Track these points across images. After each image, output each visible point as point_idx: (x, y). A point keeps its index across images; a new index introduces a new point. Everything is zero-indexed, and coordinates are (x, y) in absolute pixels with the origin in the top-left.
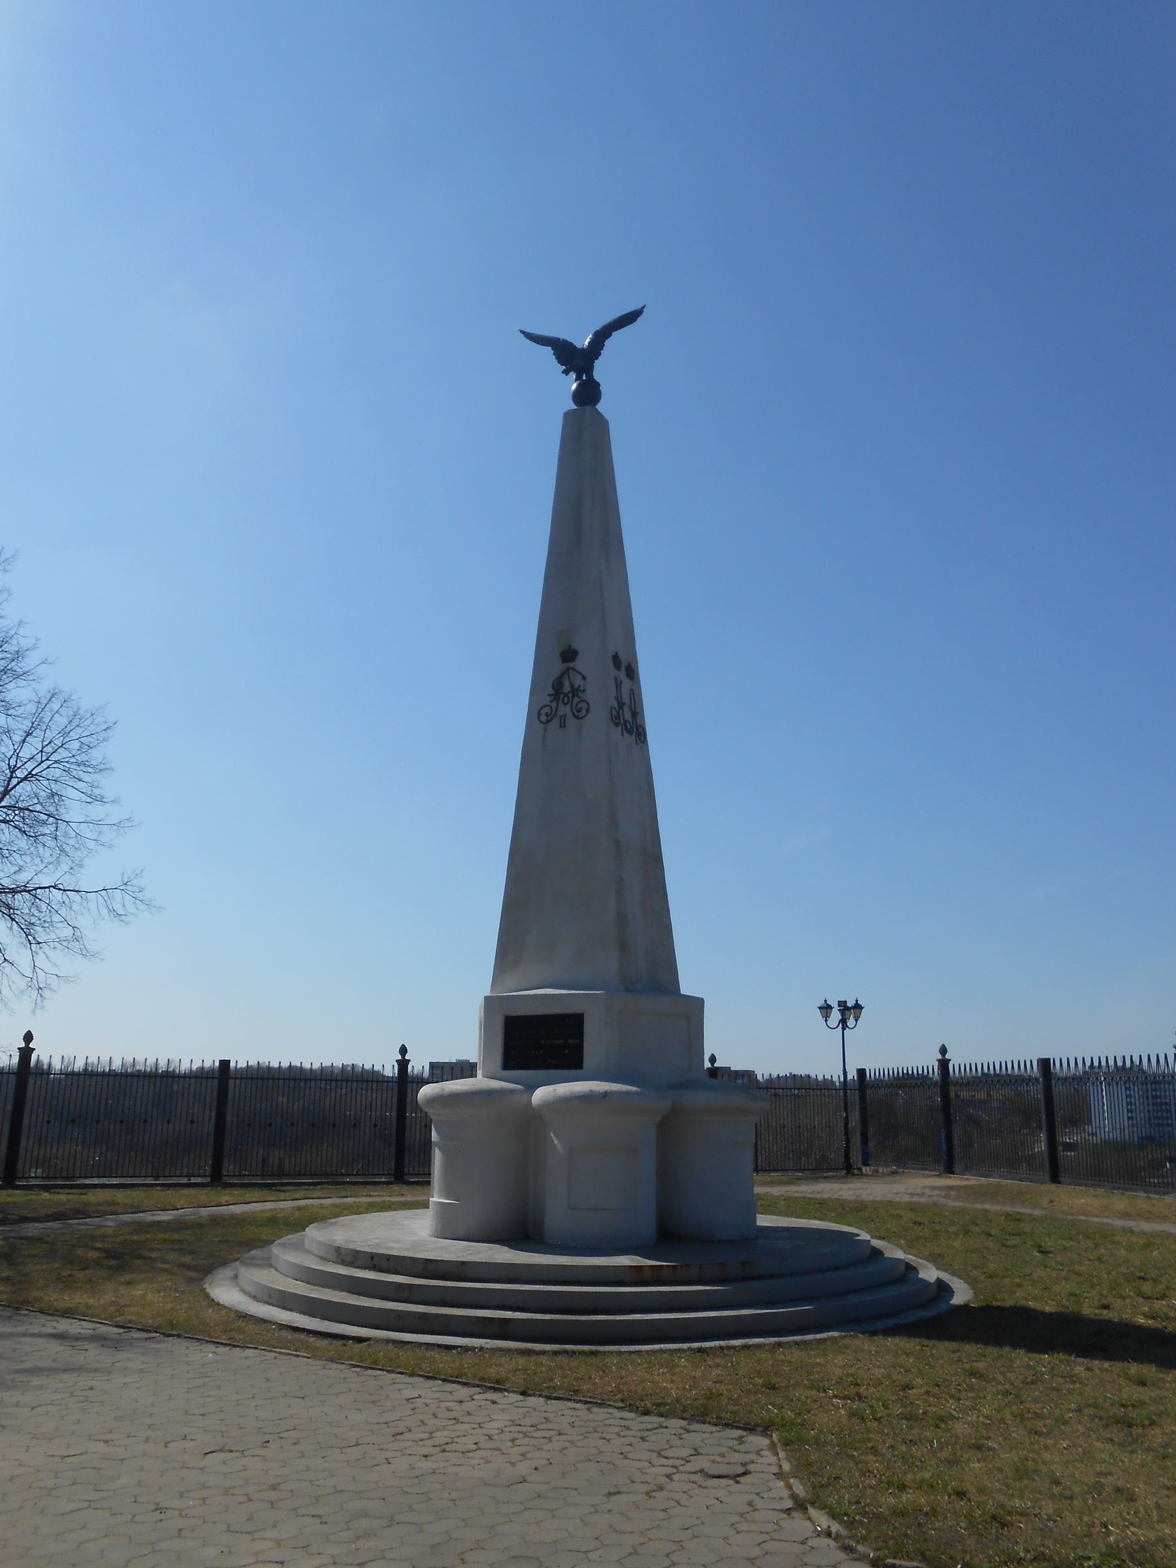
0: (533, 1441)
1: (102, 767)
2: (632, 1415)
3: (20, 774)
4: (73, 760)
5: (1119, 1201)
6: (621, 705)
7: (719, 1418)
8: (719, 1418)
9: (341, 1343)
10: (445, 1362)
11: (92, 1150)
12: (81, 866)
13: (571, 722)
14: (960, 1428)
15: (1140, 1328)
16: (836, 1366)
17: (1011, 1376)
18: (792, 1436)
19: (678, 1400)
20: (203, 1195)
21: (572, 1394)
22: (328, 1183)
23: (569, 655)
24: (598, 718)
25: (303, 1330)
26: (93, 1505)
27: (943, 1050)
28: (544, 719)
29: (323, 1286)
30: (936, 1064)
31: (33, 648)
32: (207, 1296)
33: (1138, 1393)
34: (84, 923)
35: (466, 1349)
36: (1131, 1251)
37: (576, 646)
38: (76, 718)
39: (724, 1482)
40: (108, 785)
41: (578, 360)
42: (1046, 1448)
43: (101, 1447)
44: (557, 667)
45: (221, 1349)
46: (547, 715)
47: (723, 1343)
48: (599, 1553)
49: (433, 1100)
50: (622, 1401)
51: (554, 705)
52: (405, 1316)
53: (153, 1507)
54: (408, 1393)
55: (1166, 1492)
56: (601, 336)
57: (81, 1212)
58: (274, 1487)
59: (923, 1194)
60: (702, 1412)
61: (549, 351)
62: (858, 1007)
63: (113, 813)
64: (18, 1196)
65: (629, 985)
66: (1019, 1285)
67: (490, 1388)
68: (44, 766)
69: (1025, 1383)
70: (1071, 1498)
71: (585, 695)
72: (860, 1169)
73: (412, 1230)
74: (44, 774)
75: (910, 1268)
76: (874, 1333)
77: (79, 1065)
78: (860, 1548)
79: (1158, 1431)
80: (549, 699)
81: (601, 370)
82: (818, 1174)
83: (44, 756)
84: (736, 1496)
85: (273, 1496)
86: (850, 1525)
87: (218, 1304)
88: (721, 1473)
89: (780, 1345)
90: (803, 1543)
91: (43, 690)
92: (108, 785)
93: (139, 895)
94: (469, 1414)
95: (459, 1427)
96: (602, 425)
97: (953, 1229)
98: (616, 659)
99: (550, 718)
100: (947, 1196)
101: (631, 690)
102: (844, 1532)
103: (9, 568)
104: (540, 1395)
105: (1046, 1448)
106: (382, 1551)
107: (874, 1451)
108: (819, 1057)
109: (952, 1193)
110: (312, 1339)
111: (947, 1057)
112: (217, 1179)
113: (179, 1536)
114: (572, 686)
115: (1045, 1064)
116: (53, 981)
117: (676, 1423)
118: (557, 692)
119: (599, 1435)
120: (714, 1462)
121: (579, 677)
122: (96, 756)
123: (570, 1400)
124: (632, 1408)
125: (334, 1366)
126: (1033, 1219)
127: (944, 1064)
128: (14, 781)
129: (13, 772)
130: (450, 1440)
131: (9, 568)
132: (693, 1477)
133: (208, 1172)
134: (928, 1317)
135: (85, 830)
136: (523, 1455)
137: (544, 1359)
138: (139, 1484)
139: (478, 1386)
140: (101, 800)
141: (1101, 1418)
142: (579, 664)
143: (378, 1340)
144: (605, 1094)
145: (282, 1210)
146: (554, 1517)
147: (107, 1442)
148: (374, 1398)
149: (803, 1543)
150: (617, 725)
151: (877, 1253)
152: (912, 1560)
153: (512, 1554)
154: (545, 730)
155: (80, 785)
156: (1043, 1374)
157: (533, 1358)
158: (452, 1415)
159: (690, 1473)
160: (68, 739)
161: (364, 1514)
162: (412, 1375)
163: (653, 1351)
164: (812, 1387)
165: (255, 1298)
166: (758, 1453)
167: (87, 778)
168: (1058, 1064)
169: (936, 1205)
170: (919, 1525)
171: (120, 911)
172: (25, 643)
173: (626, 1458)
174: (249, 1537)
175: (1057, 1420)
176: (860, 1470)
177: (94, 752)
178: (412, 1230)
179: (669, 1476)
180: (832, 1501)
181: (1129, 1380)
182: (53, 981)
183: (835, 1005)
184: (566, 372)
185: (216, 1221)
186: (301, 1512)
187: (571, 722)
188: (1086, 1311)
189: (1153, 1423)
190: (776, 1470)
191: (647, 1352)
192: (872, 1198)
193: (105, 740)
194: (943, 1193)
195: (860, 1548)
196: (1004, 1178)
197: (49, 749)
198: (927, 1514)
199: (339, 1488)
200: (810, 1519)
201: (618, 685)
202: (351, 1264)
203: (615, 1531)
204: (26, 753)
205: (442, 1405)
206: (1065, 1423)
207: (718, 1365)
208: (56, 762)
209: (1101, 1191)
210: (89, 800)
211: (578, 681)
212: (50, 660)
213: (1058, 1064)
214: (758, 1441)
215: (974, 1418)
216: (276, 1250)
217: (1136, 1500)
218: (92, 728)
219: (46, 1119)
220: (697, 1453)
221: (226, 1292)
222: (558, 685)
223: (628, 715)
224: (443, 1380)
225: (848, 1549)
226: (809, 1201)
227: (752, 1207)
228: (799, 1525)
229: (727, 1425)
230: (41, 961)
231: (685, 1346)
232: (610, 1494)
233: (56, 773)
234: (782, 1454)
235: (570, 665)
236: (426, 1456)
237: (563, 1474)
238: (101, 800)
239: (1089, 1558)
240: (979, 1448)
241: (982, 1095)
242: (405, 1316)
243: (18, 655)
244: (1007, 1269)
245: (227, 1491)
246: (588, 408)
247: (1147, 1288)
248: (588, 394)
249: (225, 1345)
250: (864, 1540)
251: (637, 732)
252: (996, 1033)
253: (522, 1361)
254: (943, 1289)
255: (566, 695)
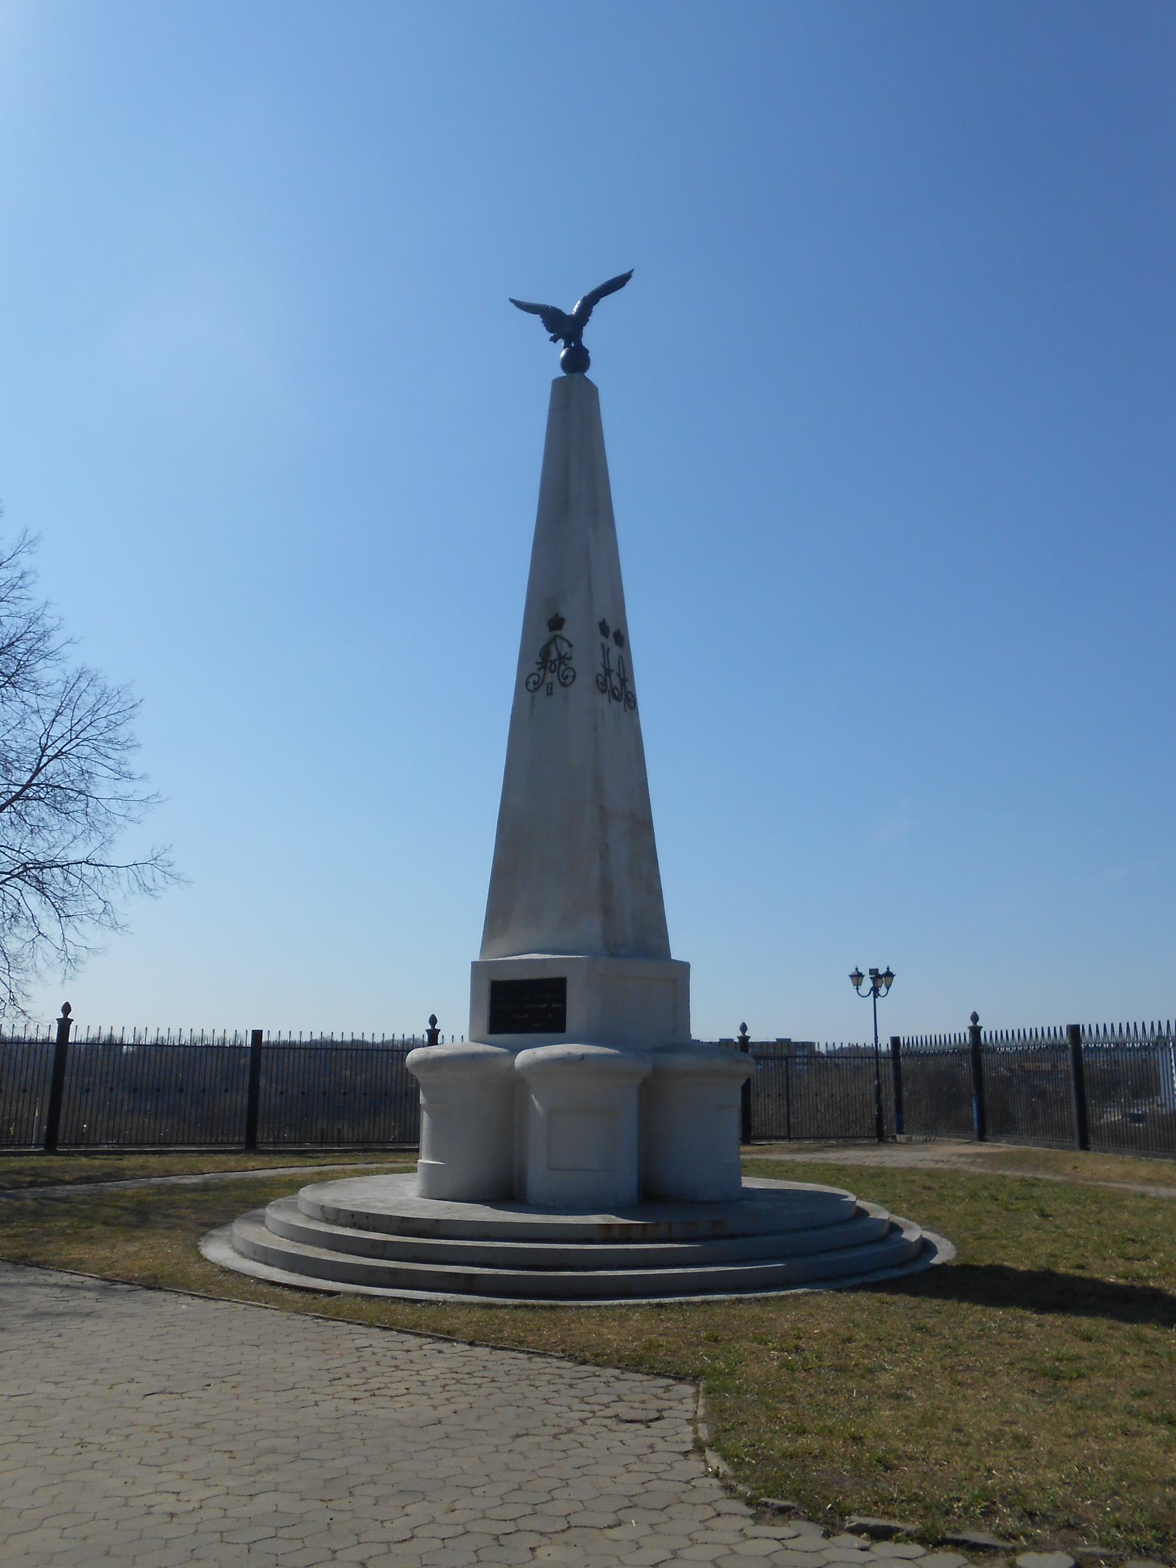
0: (464, 1387)
1: (129, 744)
2: (570, 1364)
3: (50, 752)
4: (100, 737)
5: (1143, 1168)
6: (608, 672)
7: (652, 1368)
8: (652, 1368)
9: (312, 1296)
10: (404, 1314)
11: (164, 1122)
12: (111, 842)
13: (557, 688)
14: (884, 1379)
15: (1112, 1287)
16: (787, 1320)
17: (960, 1331)
18: (714, 1384)
19: (617, 1351)
20: (232, 1161)
21: (517, 1345)
22: (359, 1151)
23: (556, 623)
24: (584, 683)
25: (279, 1284)
26: (22, 1439)
27: (975, 1018)
28: (531, 686)
29: (305, 1243)
30: (968, 1032)
31: (58, 628)
32: (198, 1252)
33: (1082, 1348)
34: (113, 897)
35: (431, 1303)
36: (1135, 1215)
37: (563, 613)
38: (104, 697)
39: (637, 1426)
40: (135, 762)
41: (566, 327)
42: (964, 1397)
43: (51, 1388)
44: (545, 634)
45: (198, 1301)
46: (535, 683)
47: (682, 1299)
48: (484, 1489)
49: (420, 1064)
50: (563, 1351)
51: (541, 673)
52: (388, 1271)
53: (78, 1441)
54: (360, 1342)
55: (1065, 1440)
56: (589, 303)
57: (110, 1176)
58: (198, 1426)
59: (949, 1161)
60: (635, 1364)
61: (537, 318)
62: (889, 975)
63: (141, 790)
64: (56, 1161)
65: (612, 949)
66: (1004, 1247)
67: (442, 1338)
68: (73, 743)
69: (970, 1337)
70: (967, 1444)
71: (575, 661)
72: (894, 1137)
73: (398, 1192)
74: (72, 751)
75: (895, 1228)
76: (840, 1290)
77: (149, 1039)
78: (740, 1488)
79: (1085, 1382)
80: (537, 667)
81: (590, 337)
82: (851, 1142)
83: (74, 735)
84: (636, 1438)
85: (194, 1433)
86: (737, 1467)
87: (206, 1260)
88: (635, 1418)
89: (740, 1301)
90: (688, 1482)
91: (71, 668)
92: (135, 762)
93: (169, 869)
94: (411, 1362)
95: (399, 1373)
96: (591, 391)
97: (961, 1193)
98: (604, 628)
99: (538, 685)
100: (973, 1163)
101: (620, 657)
102: (730, 1473)
103: (34, 549)
104: (487, 1346)
105: (964, 1397)
106: (277, 1484)
107: (793, 1400)
108: (836, 1022)
109: (979, 1160)
110: (286, 1293)
111: (978, 1024)
112: (251, 1146)
113: (92, 1468)
114: (559, 654)
115: (1074, 1031)
116: (83, 953)
117: (610, 1372)
118: (545, 660)
119: (528, 1382)
120: (632, 1408)
121: (565, 645)
122: (122, 733)
123: (514, 1350)
124: (571, 1358)
125: (298, 1317)
126: (1049, 1184)
127: (975, 1031)
128: (45, 760)
129: (43, 750)
130: (382, 1385)
131: (34, 549)
132: (608, 1422)
133: (243, 1139)
134: (907, 1273)
135: (114, 806)
136: (448, 1399)
137: (502, 1313)
138: (73, 1422)
139: (430, 1337)
140: (130, 776)
141: (1031, 1371)
142: (567, 631)
143: (347, 1294)
144: (583, 1057)
145: (304, 1174)
146: (454, 1455)
147: (56, 1383)
148: (324, 1347)
149: (688, 1482)
150: (603, 692)
151: (862, 1213)
152: (786, 1499)
153: (400, 1488)
154: (533, 698)
155: (109, 762)
156: (990, 1329)
157: (494, 1311)
158: (394, 1363)
159: (605, 1417)
160: (96, 717)
161: (274, 1451)
162: (369, 1326)
163: (612, 1306)
164: (755, 1339)
165: (241, 1254)
166: (681, 1401)
167: (111, 753)
168: (1087, 1031)
169: (957, 1171)
170: (805, 1466)
171: (150, 885)
172: (49, 623)
173: (548, 1403)
174: (158, 1469)
175: (986, 1373)
176: (768, 1417)
177: (121, 729)
178: (398, 1192)
179: (583, 1421)
180: (728, 1445)
181: (1076, 1336)
182: (83, 953)
183: (866, 972)
184: (554, 340)
185: (237, 1184)
186: (214, 1448)
187: (557, 688)
188: (1062, 1270)
189: (1081, 1376)
190: (690, 1416)
191: (606, 1307)
192: (895, 1165)
193: (131, 717)
194: (969, 1160)
195: (740, 1488)
196: (1035, 1145)
197: (78, 728)
198: (816, 1457)
199: (259, 1427)
200: (705, 1461)
201: (606, 652)
202: (334, 1222)
203: (508, 1468)
204: (56, 732)
205: (388, 1354)
206: (993, 1374)
207: (670, 1319)
208: (84, 740)
209: (1128, 1158)
210: (117, 776)
211: (565, 649)
212: (75, 640)
213: (1087, 1031)
214: (687, 1389)
215: (903, 1370)
216: (269, 1211)
217: (1030, 1448)
218: (118, 706)
219: (114, 1092)
220: (620, 1399)
221: (218, 1251)
222: (545, 653)
223: (616, 681)
224: (399, 1331)
225: (729, 1488)
226: (827, 1166)
227: (740, 1169)
228: (694, 1465)
229: (658, 1374)
230: (70, 934)
231: (644, 1301)
232: (518, 1436)
233: (86, 751)
234: (701, 1401)
235: (557, 632)
236: (355, 1399)
237: (479, 1417)
238: (130, 776)
239: (959, 1500)
240: (897, 1397)
241: (1046, 1066)
242: (388, 1271)
243: (43, 636)
244: (997, 1231)
245: (153, 1429)
246: (576, 376)
247: (1131, 1250)
248: (577, 361)
249: (202, 1297)
250: (746, 1479)
251: (626, 698)
252: (1024, 1003)
253: (479, 1314)
254: (927, 1248)
255: (553, 662)
